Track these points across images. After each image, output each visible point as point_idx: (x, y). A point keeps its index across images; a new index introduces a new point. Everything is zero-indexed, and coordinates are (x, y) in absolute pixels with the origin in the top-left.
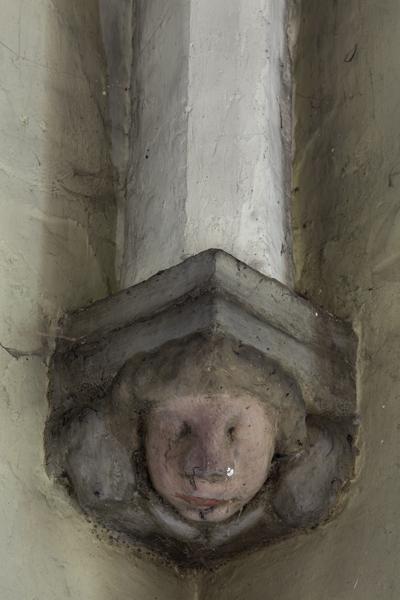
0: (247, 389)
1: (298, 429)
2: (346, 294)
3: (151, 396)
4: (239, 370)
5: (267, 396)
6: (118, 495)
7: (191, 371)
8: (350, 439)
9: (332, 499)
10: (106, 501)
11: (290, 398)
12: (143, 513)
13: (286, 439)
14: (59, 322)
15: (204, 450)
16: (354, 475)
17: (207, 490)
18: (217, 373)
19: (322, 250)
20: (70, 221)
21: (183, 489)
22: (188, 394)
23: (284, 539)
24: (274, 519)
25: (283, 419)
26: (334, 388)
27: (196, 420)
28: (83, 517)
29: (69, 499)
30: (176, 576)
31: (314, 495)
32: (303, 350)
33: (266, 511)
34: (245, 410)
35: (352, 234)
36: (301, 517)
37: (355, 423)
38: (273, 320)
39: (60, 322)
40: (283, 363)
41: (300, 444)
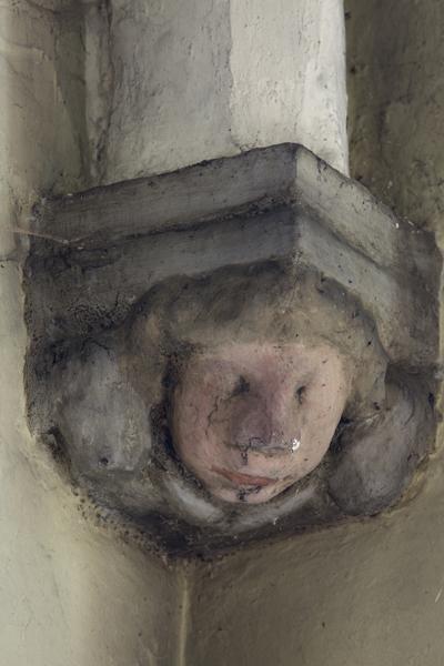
0: (327, 338)
1: (376, 388)
2: (423, 188)
3: (194, 338)
4: (320, 314)
5: (348, 347)
6: (130, 464)
7: (262, 313)
8: (432, 399)
9: (406, 480)
10: (112, 471)
11: (372, 347)
12: (151, 486)
13: (360, 401)
14: (34, 207)
15: (269, 417)
16: (434, 449)
17: (260, 465)
18: (293, 317)
19: (383, 114)
20: (35, 50)
21: (226, 462)
22: (253, 340)
23: (328, 527)
24: (325, 501)
25: (360, 375)
26: (415, 329)
27: (259, 375)
28: (69, 488)
29: (53, 464)
30: (164, 567)
31: (387, 476)
32: (383, 278)
33: (317, 492)
34: (321, 365)
35: (432, 98)
36: (367, 503)
37: (437, 377)
38: (352, 238)
39: (34, 209)
40: (363, 299)
41: (378, 408)
